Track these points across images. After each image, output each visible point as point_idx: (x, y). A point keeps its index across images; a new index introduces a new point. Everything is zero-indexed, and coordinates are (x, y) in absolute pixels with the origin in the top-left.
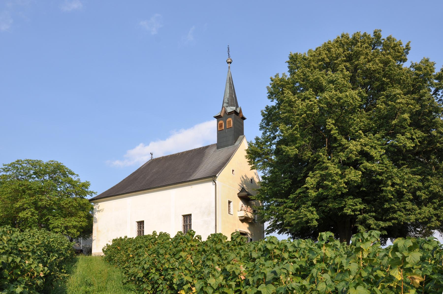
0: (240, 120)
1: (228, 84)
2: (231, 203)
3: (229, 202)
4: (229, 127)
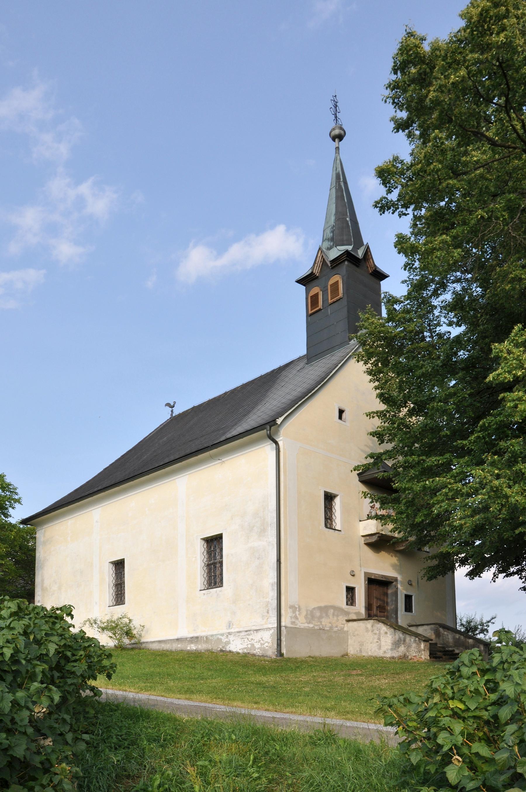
0: (371, 281)
1: (334, 190)
2: (337, 502)
3: (329, 498)
4: (335, 299)
